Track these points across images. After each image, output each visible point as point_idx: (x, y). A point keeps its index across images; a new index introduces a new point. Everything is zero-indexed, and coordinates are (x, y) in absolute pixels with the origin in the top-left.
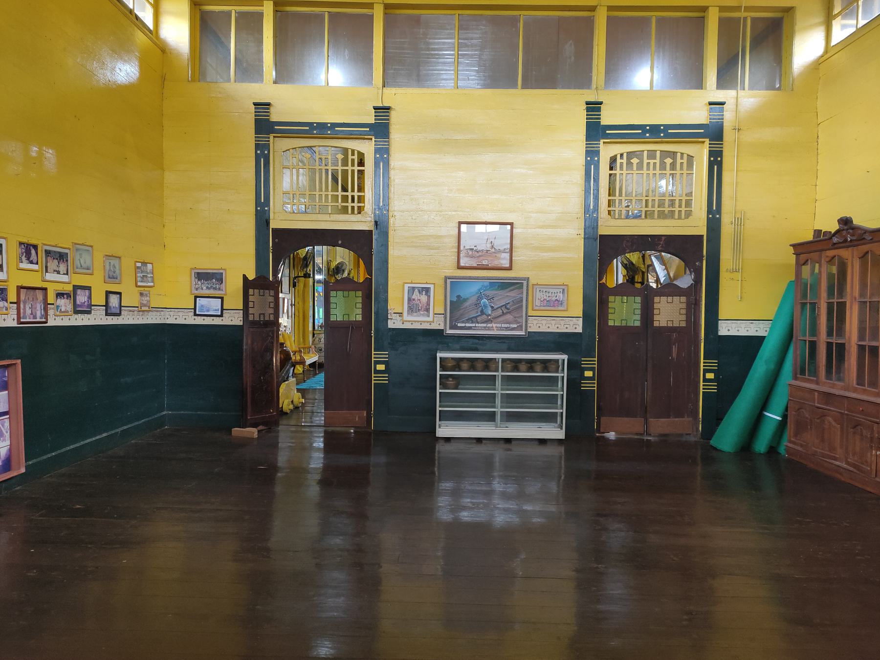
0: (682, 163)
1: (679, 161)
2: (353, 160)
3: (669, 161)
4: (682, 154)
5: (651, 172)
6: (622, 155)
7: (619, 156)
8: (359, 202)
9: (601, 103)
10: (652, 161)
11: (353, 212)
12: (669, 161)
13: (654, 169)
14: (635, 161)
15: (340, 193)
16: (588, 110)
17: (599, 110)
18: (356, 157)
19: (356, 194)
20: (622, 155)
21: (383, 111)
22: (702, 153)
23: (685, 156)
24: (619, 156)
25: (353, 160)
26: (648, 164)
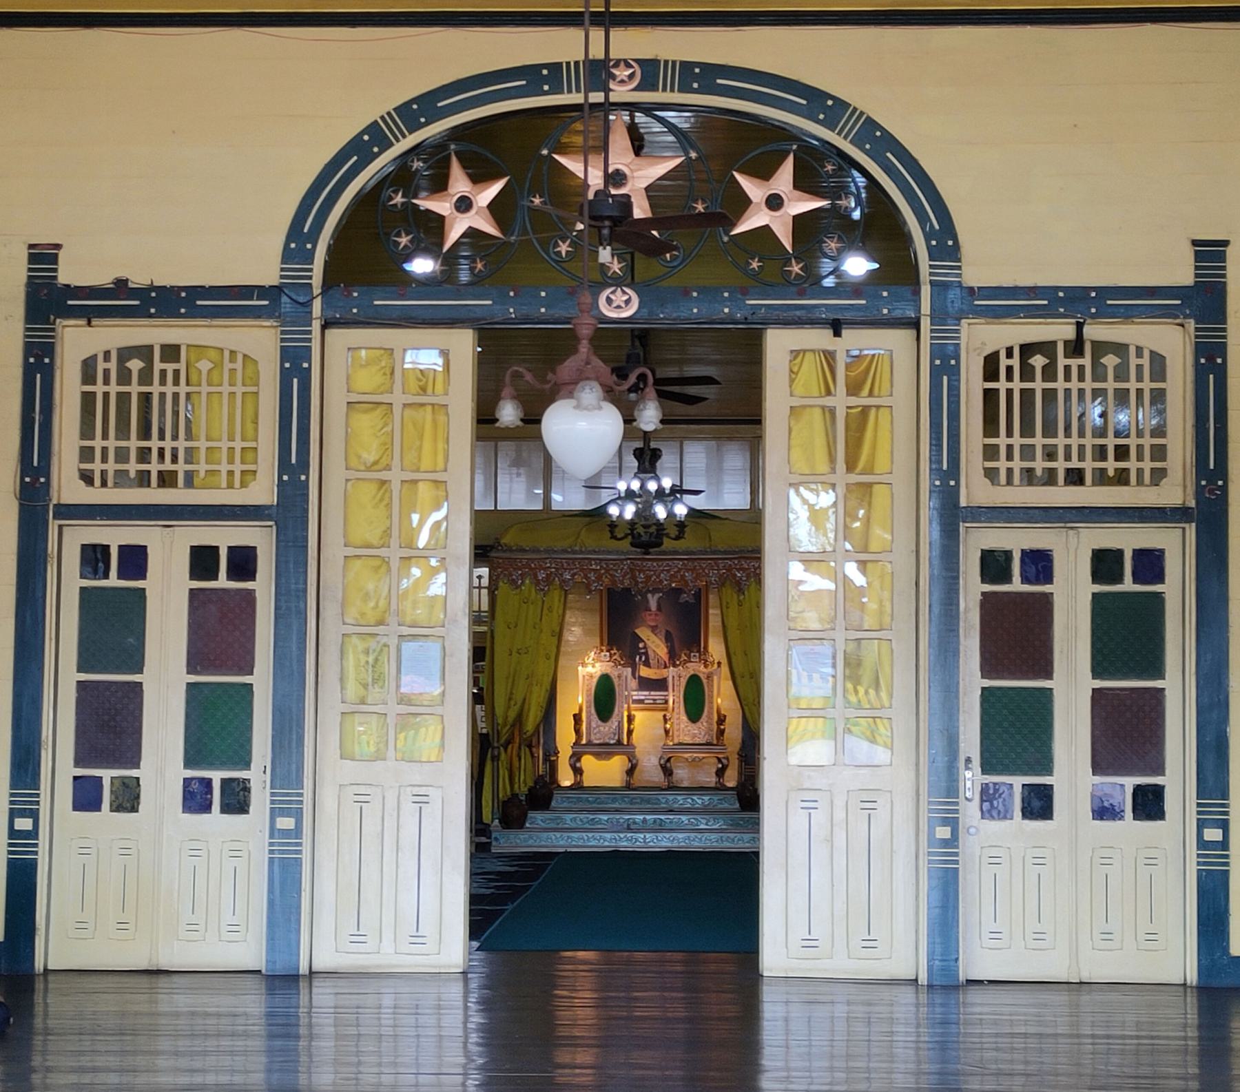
0: (233, 371)
1: (1133, 361)
2: (1139, 368)
3: (135, 365)
4: (1139, 351)
5: (1074, 385)
6: (1010, 353)
7: (1003, 354)
8: (186, 462)
9: (1225, 243)
10: (170, 367)
11: (1009, 482)
12: (135, 365)
13: (1081, 378)
14: (1038, 361)
15: (134, 443)
16: (1198, 256)
17: (1222, 257)
18: (1145, 361)
19: (182, 444)
20: (1010, 353)
21: (1210, 253)
22: (1172, 341)
23: (240, 358)
24: (1003, 354)
25: (1139, 368)
26: (163, 373)
